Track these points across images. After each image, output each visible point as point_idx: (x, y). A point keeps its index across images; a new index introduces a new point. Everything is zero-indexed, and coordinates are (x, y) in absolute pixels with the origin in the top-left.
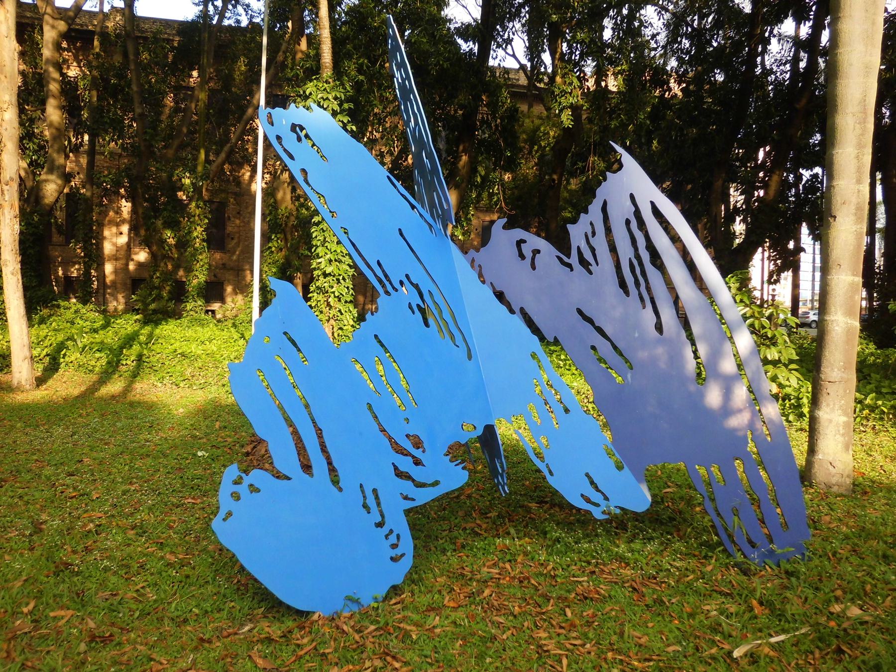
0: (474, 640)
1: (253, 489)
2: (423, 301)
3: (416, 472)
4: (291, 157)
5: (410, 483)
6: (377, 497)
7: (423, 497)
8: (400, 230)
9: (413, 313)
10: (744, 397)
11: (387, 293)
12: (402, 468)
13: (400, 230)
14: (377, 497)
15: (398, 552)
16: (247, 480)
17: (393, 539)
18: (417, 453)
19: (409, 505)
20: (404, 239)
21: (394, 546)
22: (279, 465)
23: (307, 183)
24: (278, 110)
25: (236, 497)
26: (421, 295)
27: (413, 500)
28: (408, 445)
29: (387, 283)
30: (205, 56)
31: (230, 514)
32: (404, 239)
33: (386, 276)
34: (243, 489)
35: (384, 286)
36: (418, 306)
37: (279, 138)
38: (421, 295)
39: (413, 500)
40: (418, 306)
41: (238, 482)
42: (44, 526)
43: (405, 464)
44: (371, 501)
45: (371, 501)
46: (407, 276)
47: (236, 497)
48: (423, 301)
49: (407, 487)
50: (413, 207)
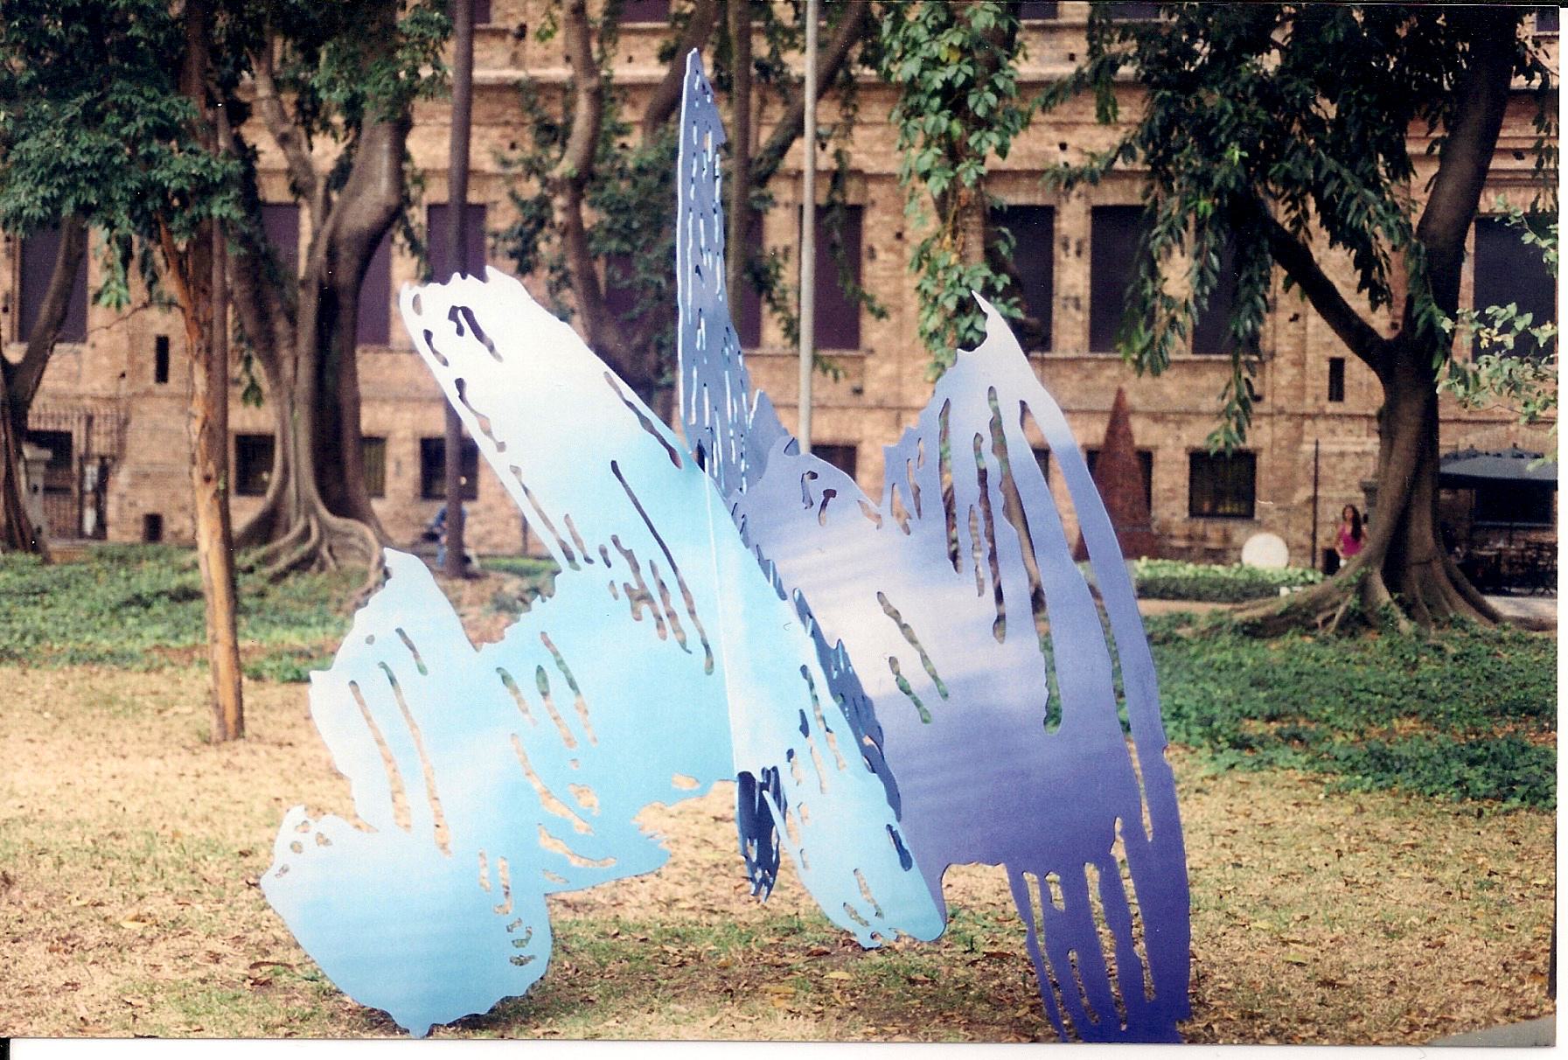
0: (896, 45)
1: (323, 840)
8: (614, 464)
9: (616, 597)
10: (1251, 733)
13: (614, 464)
15: (525, 952)
20: (625, 486)
21: (519, 943)
24: (434, 287)
25: (296, 847)
26: (636, 568)
29: (672, 586)
30: (1148, 979)
31: (284, 870)
32: (625, 486)
33: (577, 540)
34: (308, 840)
37: (428, 335)
38: (636, 568)
50: (645, 421)
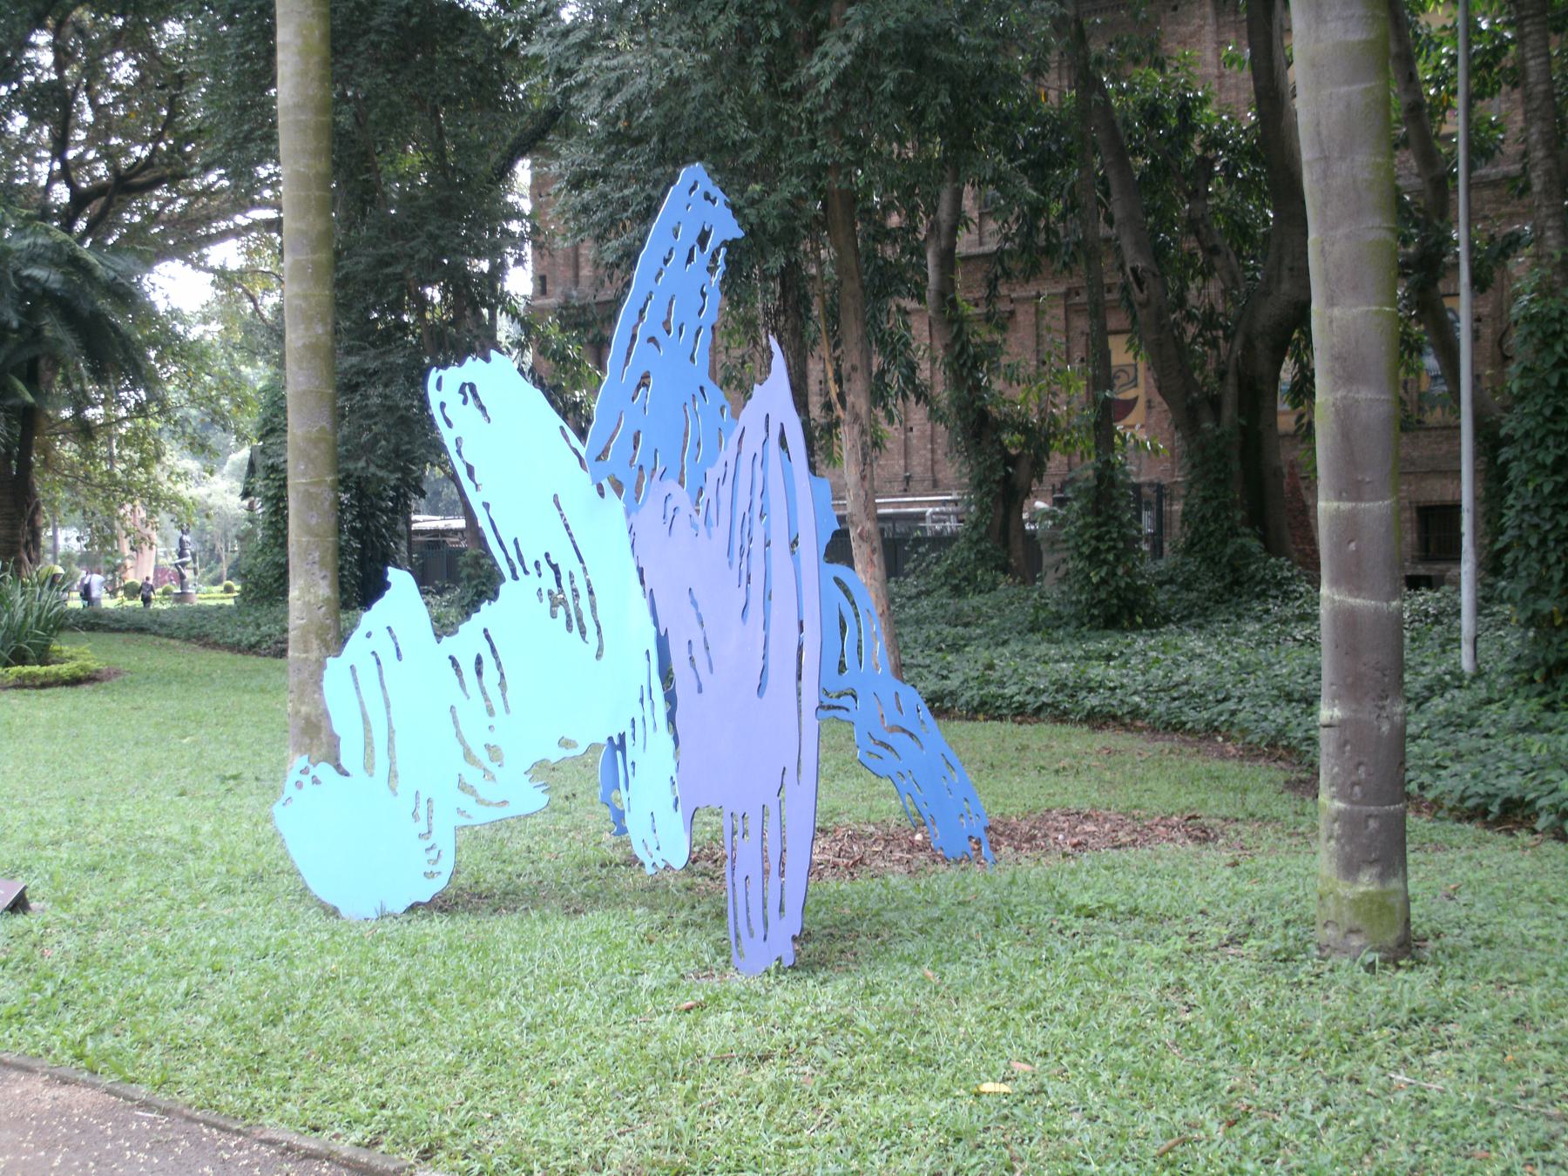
0: (377, 1024)
2: (559, 585)
3: (485, 789)
4: (449, 424)
5: (473, 799)
6: (430, 811)
7: (482, 816)
11: (515, 578)
12: (468, 780)
14: (430, 811)
15: (435, 869)
16: (313, 771)
17: (433, 854)
18: (492, 767)
19: (463, 821)
22: (344, 762)
23: (459, 452)
25: (299, 785)
27: (838, 581)
28: (481, 754)
34: (307, 780)
35: (513, 571)
36: (550, 593)
39: (838, 581)
40: (550, 593)
41: (305, 771)
42: (676, 74)
43: (473, 776)
44: (422, 812)
45: (422, 812)
46: (547, 555)
47: (299, 785)
48: (559, 585)
49: (467, 802)
